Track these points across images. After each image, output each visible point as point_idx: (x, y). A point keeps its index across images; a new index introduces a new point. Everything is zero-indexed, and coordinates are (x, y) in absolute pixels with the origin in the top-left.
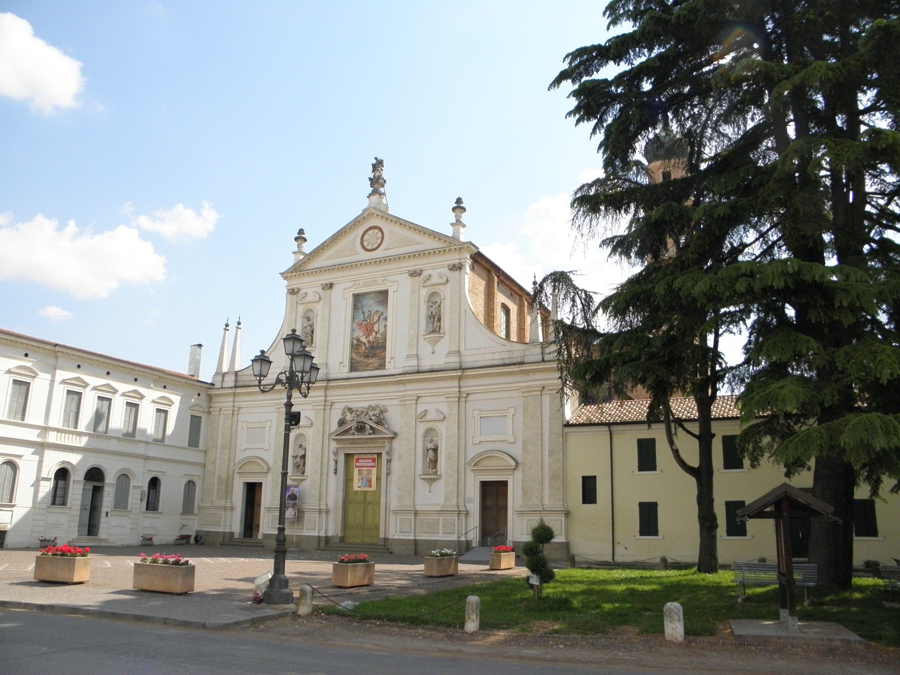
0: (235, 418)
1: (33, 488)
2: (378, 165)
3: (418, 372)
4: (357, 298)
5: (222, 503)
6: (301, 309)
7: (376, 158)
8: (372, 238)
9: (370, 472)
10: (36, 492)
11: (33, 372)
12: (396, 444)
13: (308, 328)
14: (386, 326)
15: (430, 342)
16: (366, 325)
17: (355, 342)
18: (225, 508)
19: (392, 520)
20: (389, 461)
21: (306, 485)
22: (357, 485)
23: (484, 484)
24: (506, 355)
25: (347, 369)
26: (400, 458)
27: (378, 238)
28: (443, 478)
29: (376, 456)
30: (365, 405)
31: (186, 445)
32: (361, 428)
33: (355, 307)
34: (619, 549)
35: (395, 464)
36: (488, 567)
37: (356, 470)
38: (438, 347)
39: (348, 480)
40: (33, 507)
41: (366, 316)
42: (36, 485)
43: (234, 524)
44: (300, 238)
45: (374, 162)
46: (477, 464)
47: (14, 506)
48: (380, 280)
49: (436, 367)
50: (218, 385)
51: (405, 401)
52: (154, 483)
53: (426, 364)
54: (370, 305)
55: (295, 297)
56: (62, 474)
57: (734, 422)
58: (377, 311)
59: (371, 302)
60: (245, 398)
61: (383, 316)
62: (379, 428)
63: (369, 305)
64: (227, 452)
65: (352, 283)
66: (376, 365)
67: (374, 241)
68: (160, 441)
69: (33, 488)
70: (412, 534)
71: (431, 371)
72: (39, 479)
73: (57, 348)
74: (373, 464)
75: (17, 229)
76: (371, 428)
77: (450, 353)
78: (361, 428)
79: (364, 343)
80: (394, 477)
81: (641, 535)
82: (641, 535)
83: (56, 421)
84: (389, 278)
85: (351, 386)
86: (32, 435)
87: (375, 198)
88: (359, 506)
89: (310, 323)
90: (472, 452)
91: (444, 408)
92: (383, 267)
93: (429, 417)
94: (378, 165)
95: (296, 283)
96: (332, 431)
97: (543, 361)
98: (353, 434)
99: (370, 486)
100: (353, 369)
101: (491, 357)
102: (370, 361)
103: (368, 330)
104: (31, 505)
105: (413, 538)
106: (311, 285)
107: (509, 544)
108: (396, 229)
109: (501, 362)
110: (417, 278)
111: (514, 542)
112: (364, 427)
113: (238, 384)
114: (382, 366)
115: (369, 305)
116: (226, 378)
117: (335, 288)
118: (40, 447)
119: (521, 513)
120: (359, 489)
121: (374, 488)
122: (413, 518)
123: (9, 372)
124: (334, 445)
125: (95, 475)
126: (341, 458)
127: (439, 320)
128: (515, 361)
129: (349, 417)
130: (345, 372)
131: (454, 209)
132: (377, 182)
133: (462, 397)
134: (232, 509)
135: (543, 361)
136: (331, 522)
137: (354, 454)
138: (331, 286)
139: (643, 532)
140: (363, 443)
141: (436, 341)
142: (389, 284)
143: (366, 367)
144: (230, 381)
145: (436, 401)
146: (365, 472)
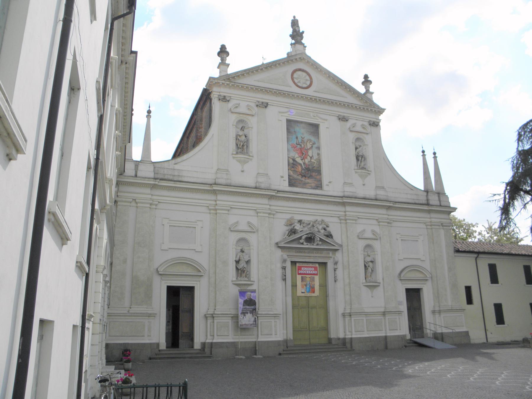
2: (295, 23)
3: (376, 200)
7: (294, 17)
9: (313, 280)
12: (338, 256)
13: (243, 138)
15: (239, 161)
17: (291, 161)
18: (149, 315)
20: (335, 270)
22: (300, 290)
23: (408, 291)
28: (381, 285)
29: (317, 265)
32: (310, 239)
33: (288, 131)
34: (489, 335)
35: (339, 273)
37: (299, 277)
41: (300, 140)
44: (223, 52)
49: (368, 196)
53: (361, 193)
54: (302, 133)
59: (302, 131)
62: (328, 240)
65: (287, 110)
66: (313, 185)
70: (384, 331)
71: (364, 198)
75: (303, 32)
79: (300, 164)
84: (319, 115)
87: (298, 46)
88: (310, 310)
90: (400, 266)
91: (254, 221)
94: (295, 23)
96: (277, 240)
97: (440, 206)
98: (302, 244)
99: (314, 292)
100: (291, 184)
103: (303, 153)
105: (384, 335)
109: (413, 202)
110: (345, 123)
112: (314, 239)
114: (319, 186)
116: (141, 167)
119: (210, 317)
120: (303, 295)
121: (317, 293)
126: (288, 265)
129: (298, 227)
130: (284, 185)
134: (434, 312)
135: (136, 176)
142: (320, 120)
145: (366, 224)
146: (308, 279)
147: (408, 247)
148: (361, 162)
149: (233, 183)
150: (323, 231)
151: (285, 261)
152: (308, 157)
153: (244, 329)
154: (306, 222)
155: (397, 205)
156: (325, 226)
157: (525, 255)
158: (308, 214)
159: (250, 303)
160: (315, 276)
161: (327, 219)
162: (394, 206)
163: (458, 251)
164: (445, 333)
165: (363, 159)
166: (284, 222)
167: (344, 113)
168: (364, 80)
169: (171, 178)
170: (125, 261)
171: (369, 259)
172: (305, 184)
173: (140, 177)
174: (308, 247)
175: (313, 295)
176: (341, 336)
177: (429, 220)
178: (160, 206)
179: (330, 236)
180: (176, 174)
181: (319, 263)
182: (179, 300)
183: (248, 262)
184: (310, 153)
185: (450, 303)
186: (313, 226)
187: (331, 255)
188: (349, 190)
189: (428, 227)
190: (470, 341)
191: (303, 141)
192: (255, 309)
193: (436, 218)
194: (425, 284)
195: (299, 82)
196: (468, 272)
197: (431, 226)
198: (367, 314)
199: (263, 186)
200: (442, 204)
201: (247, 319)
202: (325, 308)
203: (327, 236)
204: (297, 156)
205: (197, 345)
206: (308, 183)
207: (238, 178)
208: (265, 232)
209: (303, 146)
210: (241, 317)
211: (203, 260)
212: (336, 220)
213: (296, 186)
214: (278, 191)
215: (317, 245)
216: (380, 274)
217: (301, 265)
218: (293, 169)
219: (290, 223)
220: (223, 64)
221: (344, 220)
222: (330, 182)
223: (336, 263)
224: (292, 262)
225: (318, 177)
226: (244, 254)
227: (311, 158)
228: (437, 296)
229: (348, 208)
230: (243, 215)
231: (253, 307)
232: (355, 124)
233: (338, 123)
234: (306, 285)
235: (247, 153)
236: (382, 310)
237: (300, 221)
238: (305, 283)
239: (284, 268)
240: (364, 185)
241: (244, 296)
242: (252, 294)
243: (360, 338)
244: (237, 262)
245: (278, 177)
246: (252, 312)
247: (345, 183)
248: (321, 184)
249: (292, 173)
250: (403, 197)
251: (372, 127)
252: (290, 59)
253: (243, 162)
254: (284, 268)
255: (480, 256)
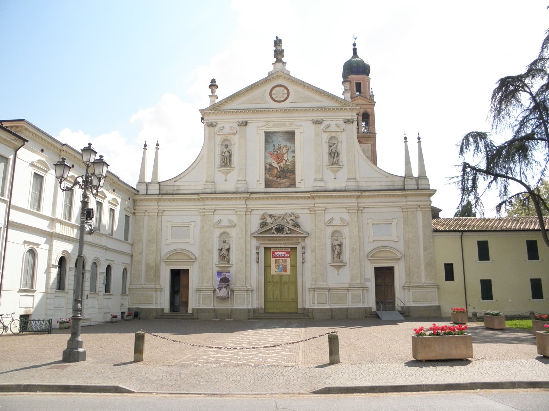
0: (160, 218)
1: (45, 274)
2: (278, 42)
4: (268, 136)
5: (152, 285)
6: (219, 139)
7: (277, 37)
8: (279, 93)
10: (48, 278)
11: (47, 166)
12: (308, 241)
13: (227, 154)
14: (294, 157)
15: (223, 173)
16: (277, 155)
17: (268, 166)
18: (156, 290)
19: (308, 296)
20: (303, 253)
21: (233, 270)
22: (274, 270)
23: (377, 269)
24: (390, 184)
25: (263, 185)
26: (313, 251)
27: (284, 94)
28: (348, 265)
29: (289, 250)
30: (282, 212)
31: (123, 239)
32: (280, 229)
33: (267, 141)
35: (308, 256)
36: (483, 324)
37: (273, 260)
38: (339, 174)
39: (267, 267)
40: (46, 293)
41: (276, 147)
42: (48, 272)
43: (163, 301)
44: (213, 85)
45: (275, 39)
46: (371, 256)
47: (34, 291)
48: (288, 123)
49: (338, 189)
50: (143, 192)
51: (204, 212)
52: (109, 268)
53: (331, 185)
55: (212, 129)
56: (62, 261)
57: (537, 233)
58: (286, 146)
59: (280, 139)
60: (168, 203)
61: (291, 150)
63: (279, 142)
64: (155, 246)
65: (265, 124)
66: (287, 184)
67: (281, 95)
68: (110, 235)
69: (45, 274)
70: (212, 305)
71: (335, 191)
72: (49, 267)
73: (64, 147)
74: (288, 255)
76: (289, 229)
77: (349, 179)
78: (280, 229)
79: (276, 168)
80: (308, 265)
81: (483, 299)
82: (483, 299)
83: (60, 214)
84: (295, 123)
85: (268, 198)
86: (43, 225)
87: (279, 65)
89: (228, 149)
90: (369, 248)
91: (346, 217)
92: (290, 115)
93: (334, 223)
94: (278, 42)
95: (211, 118)
96: (253, 231)
97: (418, 189)
98: (273, 233)
99: (286, 271)
100: (267, 186)
101: (379, 184)
102: (282, 181)
103: (279, 158)
104: (44, 290)
105: (213, 308)
106: (228, 123)
107: (398, 308)
108: (300, 89)
109: (387, 188)
110: (319, 125)
111: (193, 309)
112: (283, 229)
113: (162, 192)
114: (293, 185)
115: (279, 142)
116: (150, 187)
117: (249, 124)
118: (50, 236)
119: (199, 290)
120: (276, 274)
121: (289, 272)
122: (212, 294)
123: (32, 164)
124: (255, 242)
125: (80, 262)
126: (262, 251)
127: (338, 155)
128: (397, 188)
129: (269, 220)
130: (261, 187)
131: (210, 86)
132: (279, 54)
133: (360, 210)
134: (161, 290)
135: (147, 194)
136: (255, 299)
137: (270, 248)
138: (246, 124)
139: (483, 298)
140: (280, 240)
141: (226, 173)
142: (295, 127)
143: (279, 185)
144: (154, 189)
145: (338, 212)
147: (385, 231)
148: (334, 158)
149: (217, 191)
150: (290, 222)
151: (258, 248)
152: (284, 162)
153: (223, 300)
154: (277, 215)
155: (367, 193)
156: (293, 218)
157: (445, 231)
158: (280, 207)
159: (225, 281)
160: (287, 259)
161: (296, 212)
162: (364, 194)
163: (436, 231)
164: (411, 307)
165: (336, 155)
166: (259, 217)
167: (318, 116)
168: (343, 80)
169: (172, 192)
170: (141, 253)
171: (336, 243)
172: (280, 184)
173: (407, 190)
174: (279, 237)
175: (285, 273)
176: (307, 306)
177: (405, 204)
178: (366, 210)
179: (297, 225)
180: (176, 188)
181: (291, 248)
182: (179, 278)
183: (228, 250)
184: (285, 157)
185: (423, 280)
186: (284, 218)
187: (300, 241)
188: (319, 185)
189: (404, 210)
190: (441, 315)
191: (279, 148)
192: (229, 285)
193: (412, 202)
194: (396, 263)
195: (277, 97)
196: (448, 250)
197: (407, 209)
198: (330, 290)
199: (240, 190)
200: (420, 187)
201: (223, 292)
202: (295, 283)
203: (295, 226)
204: (273, 161)
205: (190, 311)
206: (283, 183)
207: (222, 186)
208: (240, 226)
209: (279, 152)
210: (218, 291)
211: (195, 250)
212: (307, 211)
213: (272, 187)
214: (251, 193)
215: (287, 233)
216: (347, 255)
217: (274, 250)
218: (269, 173)
219: (263, 217)
220: (213, 96)
221: (313, 211)
222: (302, 180)
223: (303, 248)
224: (265, 248)
225: (292, 176)
226: (225, 244)
227: (286, 161)
228: (409, 274)
229: (318, 201)
230: (227, 214)
231: (227, 284)
232: (330, 125)
233: (313, 127)
234: (279, 266)
235: (230, 165)
236: (347, 286)
237: (271, 216)
238: (278, 264)
239: (258, 253)
240: (335, 178)
241: (221, 276)
242: (227, 274)
243: (342, 309)
244: (221, 250)
245: (256, 179)
246: (226, 287)
247: (348, 179)
248: (295, 183)
249: (268, 176)
250: (384, 185)
251: (347, 125)
252: (271, 77)
253: (335, 172)
254: (258, 253)
255: (465, 234)
